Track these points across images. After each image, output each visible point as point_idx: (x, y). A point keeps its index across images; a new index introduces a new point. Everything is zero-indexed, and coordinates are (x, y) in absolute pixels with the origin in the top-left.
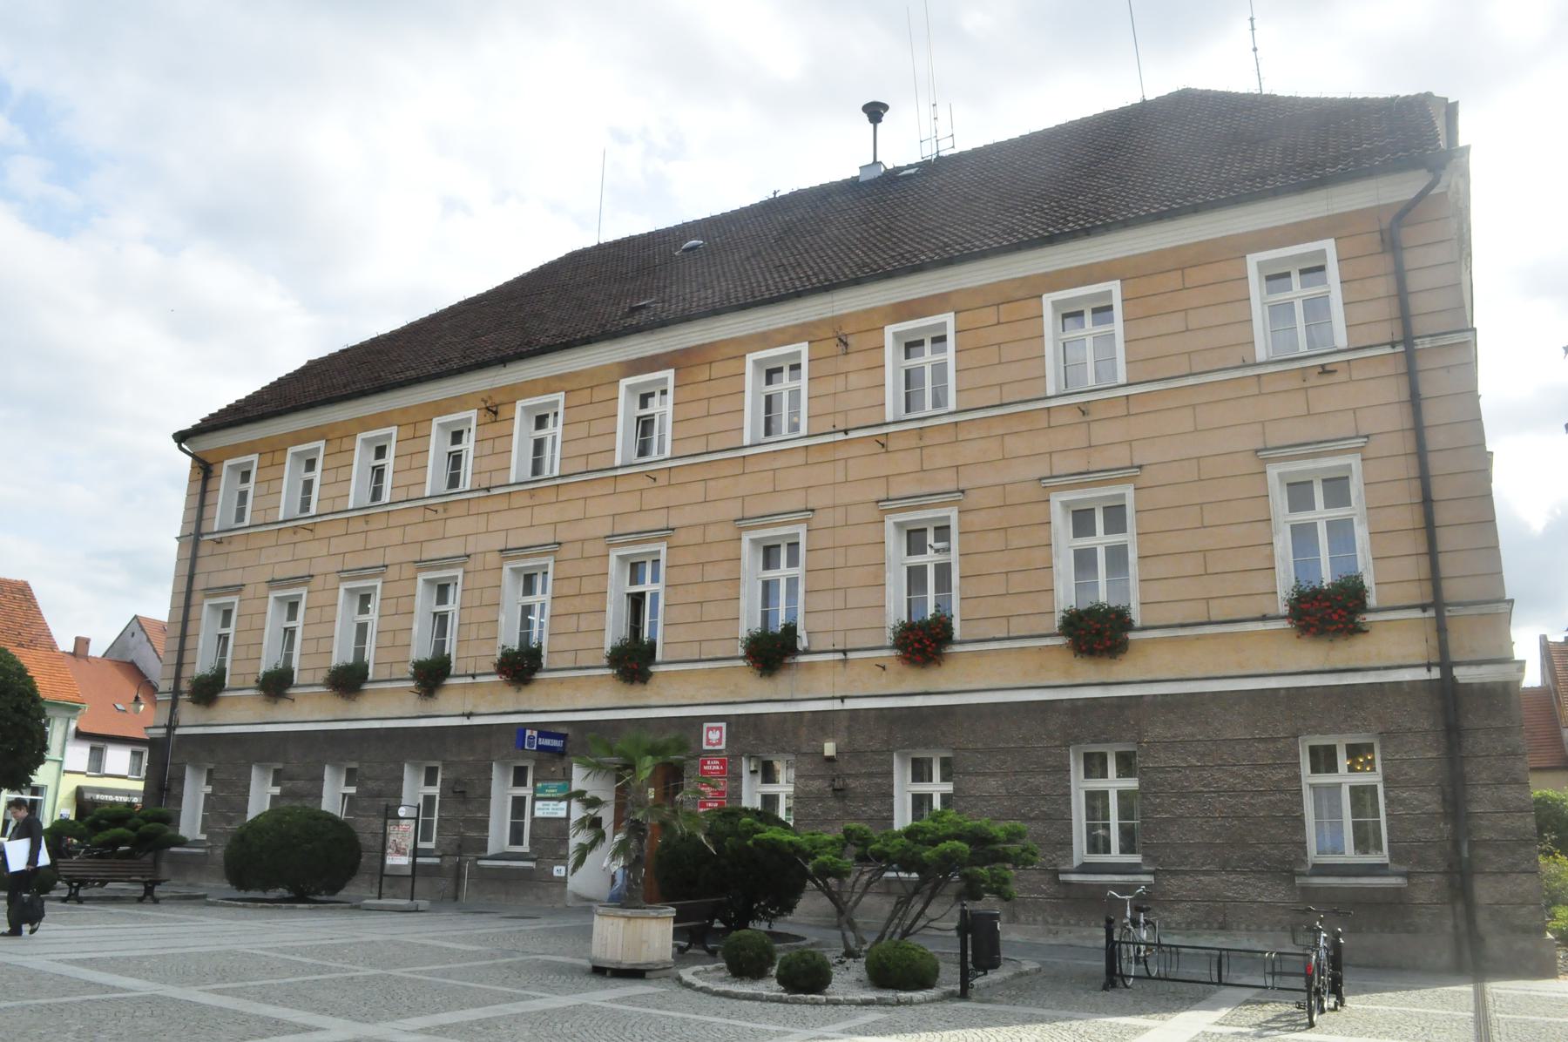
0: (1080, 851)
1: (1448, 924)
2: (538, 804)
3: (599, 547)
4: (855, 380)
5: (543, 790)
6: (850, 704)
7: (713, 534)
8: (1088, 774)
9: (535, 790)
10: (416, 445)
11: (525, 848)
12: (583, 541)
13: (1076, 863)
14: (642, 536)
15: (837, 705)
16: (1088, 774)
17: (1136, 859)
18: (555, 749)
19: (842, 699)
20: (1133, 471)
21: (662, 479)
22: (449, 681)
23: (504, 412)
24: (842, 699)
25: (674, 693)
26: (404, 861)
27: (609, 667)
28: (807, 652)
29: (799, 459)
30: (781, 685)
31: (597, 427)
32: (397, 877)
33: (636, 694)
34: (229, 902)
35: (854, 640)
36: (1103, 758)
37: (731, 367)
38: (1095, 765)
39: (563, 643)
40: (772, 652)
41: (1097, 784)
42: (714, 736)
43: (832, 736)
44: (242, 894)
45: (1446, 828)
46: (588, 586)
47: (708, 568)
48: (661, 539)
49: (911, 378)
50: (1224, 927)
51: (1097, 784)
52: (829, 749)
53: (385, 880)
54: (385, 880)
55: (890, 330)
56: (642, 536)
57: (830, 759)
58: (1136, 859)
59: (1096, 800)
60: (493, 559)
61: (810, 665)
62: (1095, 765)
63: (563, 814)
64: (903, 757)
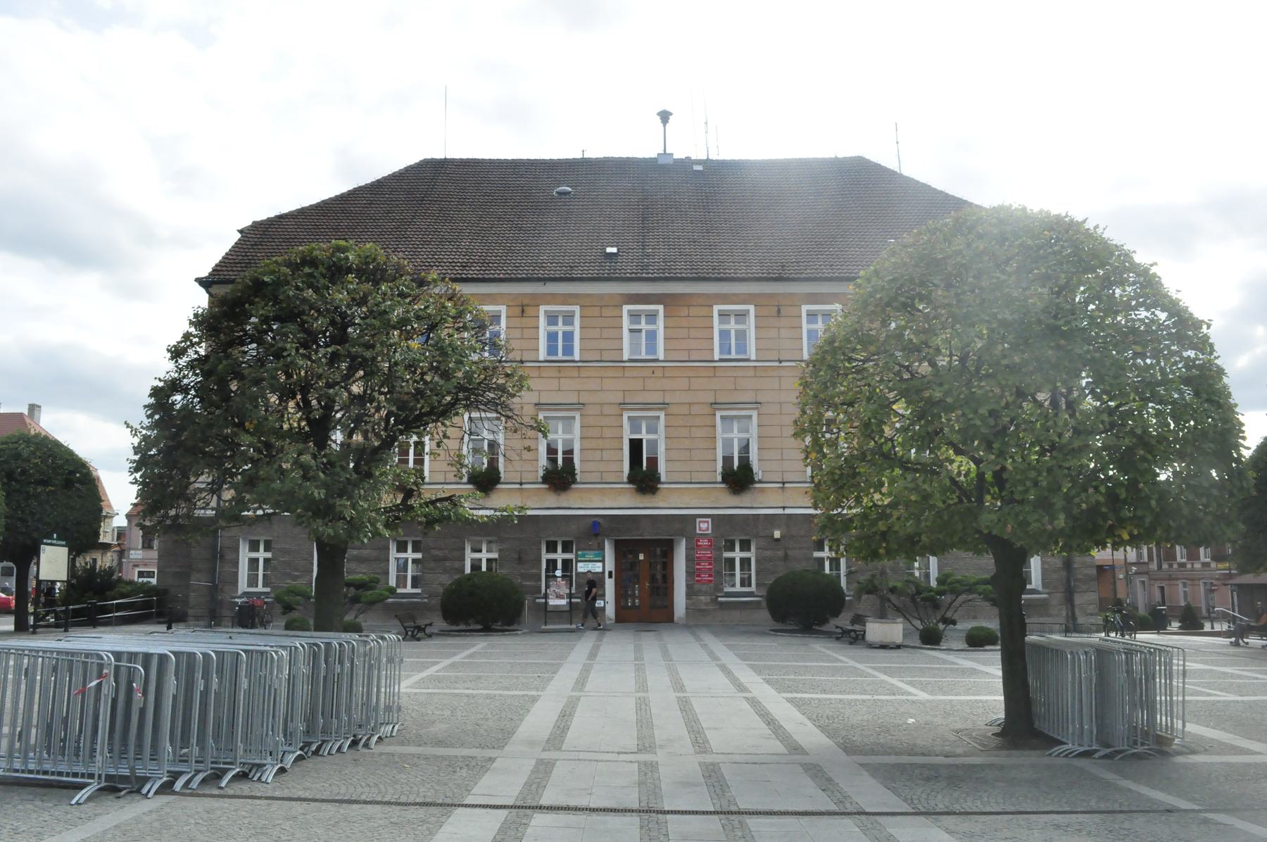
0: (243, 586)
1: (1064, 613)
2: (580, 564)
3: (615, 410)
4: (784, 333)
5: (583, 556)
6: (788, 511)
7: (608, 410)
8: (398, 551)
9: (577, 556)
10: (526, 321)
11: (753, 588)
12: (602, 404)
13: (240, 592)
14: (646, 406)
15: (780, 511)
16: (398, 551)
17: (418, 591)
18: (594, 531)
19: (784, 508)
20: (663, 405)
21: (659, 373)
22: (499, 486)
23: (529, 311)
24: (784, 508)
25: (675, 500)
26: (563, 602)
27: (543, 483)
28: (760, 482)
29: (751, 373)
30: (745, 499)
31: (527, 333)
32: (558, 613)
33: (647, 500)
34: (444, 634)
35: (788, 477)
36: (555, 543)
37: (615, 312)
38: (254, 546)
39: (590, 466)
40: (739, 478)
41: (552, 556)
42: (704, 526)
43: (779, 528)
44: (454, 628)
45: (1064, 574)
46: (608, 433)
47: (693, 429)
48: (660, 409)
49: (552, 337)
50: (975, 617)
51: (552, 556)
52: (777, 534)
53: (547, 613)
54: (547, 613)
55: (542, 309)
56: (646, 406)
57: (777, 540)
58: (418, 591)
59: (254, 562)
60: (614, 410)
61: (762, 490)
62: (402, 547)
63: (600, 570)
64: (244, 539)
